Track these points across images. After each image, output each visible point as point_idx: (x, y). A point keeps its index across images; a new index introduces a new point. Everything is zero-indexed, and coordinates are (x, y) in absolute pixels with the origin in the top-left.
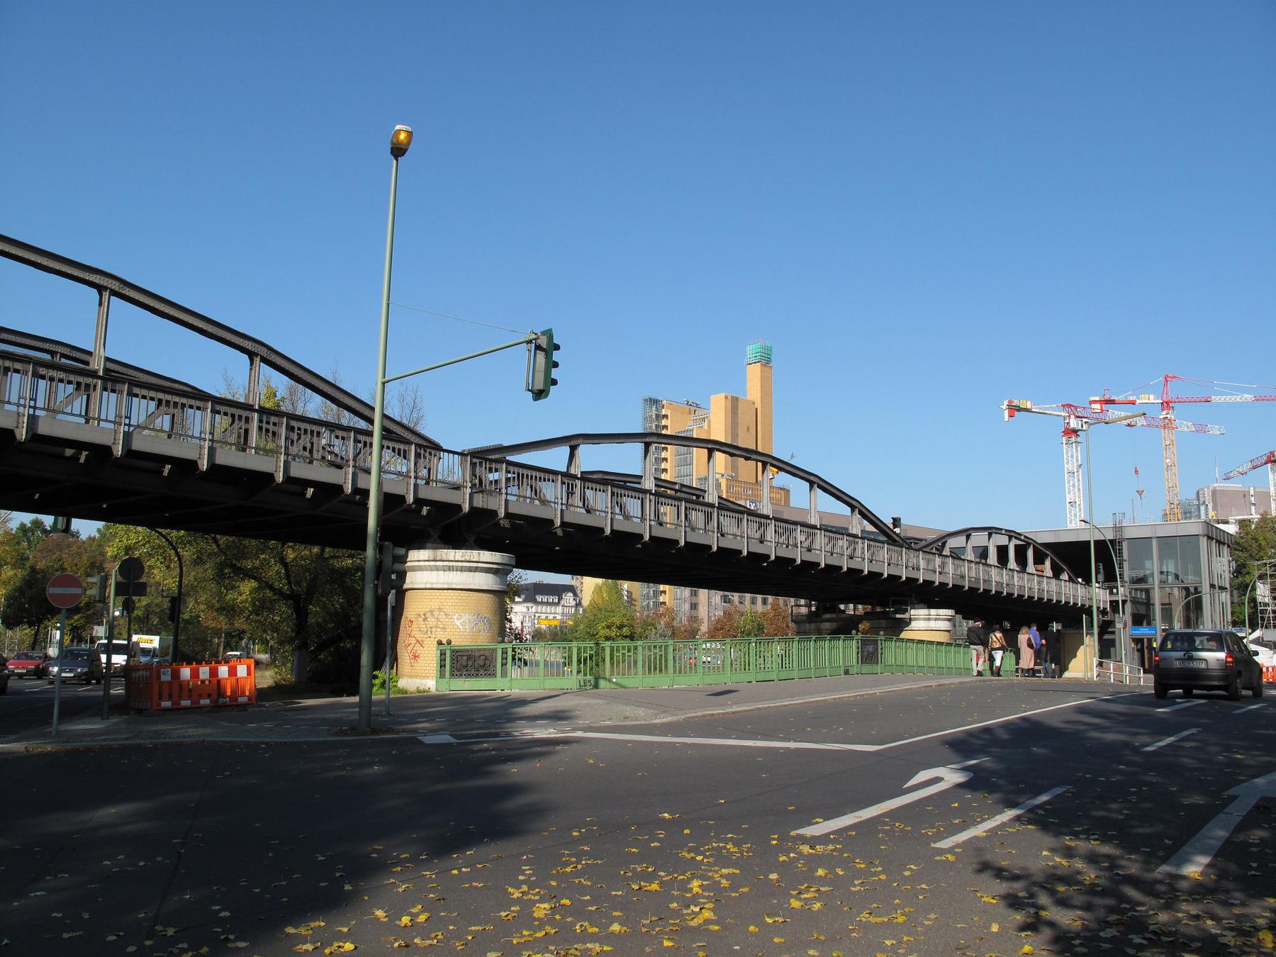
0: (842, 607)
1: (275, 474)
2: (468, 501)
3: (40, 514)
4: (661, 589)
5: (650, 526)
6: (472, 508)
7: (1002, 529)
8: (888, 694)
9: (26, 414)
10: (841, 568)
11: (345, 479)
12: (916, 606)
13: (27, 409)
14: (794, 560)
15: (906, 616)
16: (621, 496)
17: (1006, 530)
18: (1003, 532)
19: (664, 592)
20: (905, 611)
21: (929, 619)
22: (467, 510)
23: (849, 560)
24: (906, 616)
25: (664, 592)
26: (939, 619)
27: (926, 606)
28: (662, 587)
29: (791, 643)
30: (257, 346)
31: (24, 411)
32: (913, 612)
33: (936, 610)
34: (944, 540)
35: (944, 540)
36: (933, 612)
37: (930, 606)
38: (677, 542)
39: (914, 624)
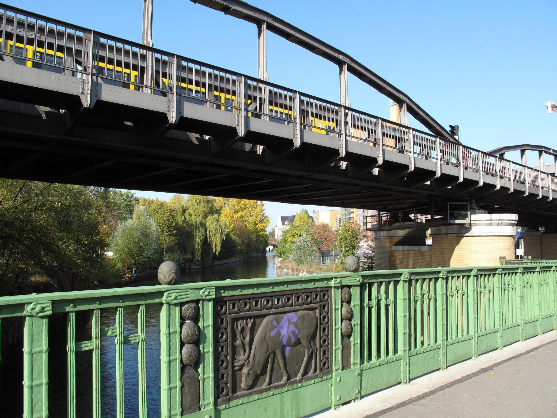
0: (412, 216)
1: (238, 128)
2: (243, 124)
3: (122, 189)
4: (352, 211)
5: (414, 158)
6: (303, 144)
7: (550, 149)
8: (186, 389)
9: (90, 81)
10: (477, 182)
11: (340, 145)
12: (477, 211)
13: (90, 76)
14: (477, 182)
15: (466, 221)
16: (308, 116)
17: (554, 150)
18: (551, 151)
19: (353, 212)
20: (465, 217)
21: (491, 224)
22: (243, 133)
23: (465, 170)
24: (466, 221)
25: (353, 212)
26: (501, 224)
27: (487, 211)
28: (352, 210)
29: (391, 287)
30: (404, 97)
31: (88, 78)
32: (474, 217)
33: (498, 214)
34: (502, 152)
35: (502, 152)
36: (495, 216)
37: (491, 211)
38: (407, 167)
39: (474, 230)
